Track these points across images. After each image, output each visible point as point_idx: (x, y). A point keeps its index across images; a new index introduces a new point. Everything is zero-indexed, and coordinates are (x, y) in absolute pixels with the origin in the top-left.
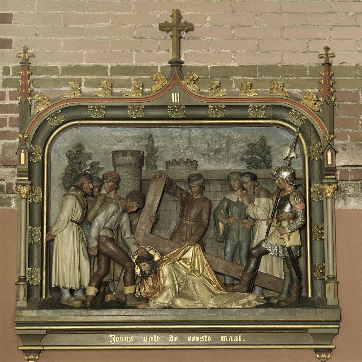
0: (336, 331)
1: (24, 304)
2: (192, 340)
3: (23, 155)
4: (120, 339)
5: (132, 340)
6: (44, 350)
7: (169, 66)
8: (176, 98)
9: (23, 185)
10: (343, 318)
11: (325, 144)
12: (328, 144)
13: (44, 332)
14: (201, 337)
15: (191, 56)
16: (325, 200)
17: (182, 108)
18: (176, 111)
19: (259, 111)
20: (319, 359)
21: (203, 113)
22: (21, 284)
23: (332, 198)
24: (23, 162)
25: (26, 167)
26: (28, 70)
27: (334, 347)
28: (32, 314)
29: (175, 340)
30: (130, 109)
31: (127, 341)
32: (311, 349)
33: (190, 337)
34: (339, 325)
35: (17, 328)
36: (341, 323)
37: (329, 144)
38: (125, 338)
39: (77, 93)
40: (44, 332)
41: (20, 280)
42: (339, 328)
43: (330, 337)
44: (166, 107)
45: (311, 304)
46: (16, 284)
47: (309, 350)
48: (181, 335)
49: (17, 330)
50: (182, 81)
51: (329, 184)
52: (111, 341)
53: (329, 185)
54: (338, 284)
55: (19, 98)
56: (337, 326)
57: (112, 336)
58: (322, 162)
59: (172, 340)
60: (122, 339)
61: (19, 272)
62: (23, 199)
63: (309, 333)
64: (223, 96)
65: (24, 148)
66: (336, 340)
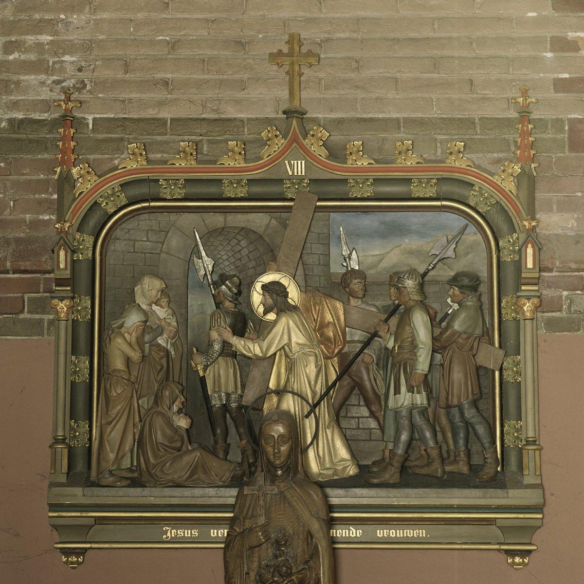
0: (539, 523)
1: (63, 479)
2: (342, 535)
3: (62, 253)
4: (179, 533)
5: (197, 535)
6: (90, 548)
7: (282, 119)
8: (299, 167)
9: (62, 299)
10: (547, 502)
11: (523, 237)
12: (61, 238)
13: (92, 521)
14: (179, 531)
15: (318, 104)
16: (522, 322)
17: (181, 184)
18: (295, 188)
19: (238, 187)
20: (67, 562)
21: (213, 190)
22: (530, 449)
23: (532, 319)
24: (62, 266)
25: (68, 272)
26: (72, 128)
27: (536, 548)
28: (78, 494)
29: (358, 535)
30: (162, 185)
31: (189, 535)
32: (499, 550)
33: (175, 530)
34: (542, 513)
35: (51, 514)
36: (545, 509)
37: (62, 238)
38: (186, 531)
39: (190, 160)
40: (92, 521)
41: (57, 441)
42: (542, 519)
43: (529, 530)
44: (280, 181)
45: (497, 482)
46: (50, 447)
47: (493, 552)
48: (366, 527)
49: (50, 517)
50: (305, 138)
51: (528, 298)
52: (165, 536)
53: (62, 300)
54: (542, 451)
55: (58, 170)
56: (540, 516)
57: (167, 528)
58: (519, 265)
59: (216, 535)
60: (196, 533)
61: (56, 430)
62: (529, 319)
63: (498, 527)
64: (368, 164)
65: (532, 242)
66: (538, 537)
